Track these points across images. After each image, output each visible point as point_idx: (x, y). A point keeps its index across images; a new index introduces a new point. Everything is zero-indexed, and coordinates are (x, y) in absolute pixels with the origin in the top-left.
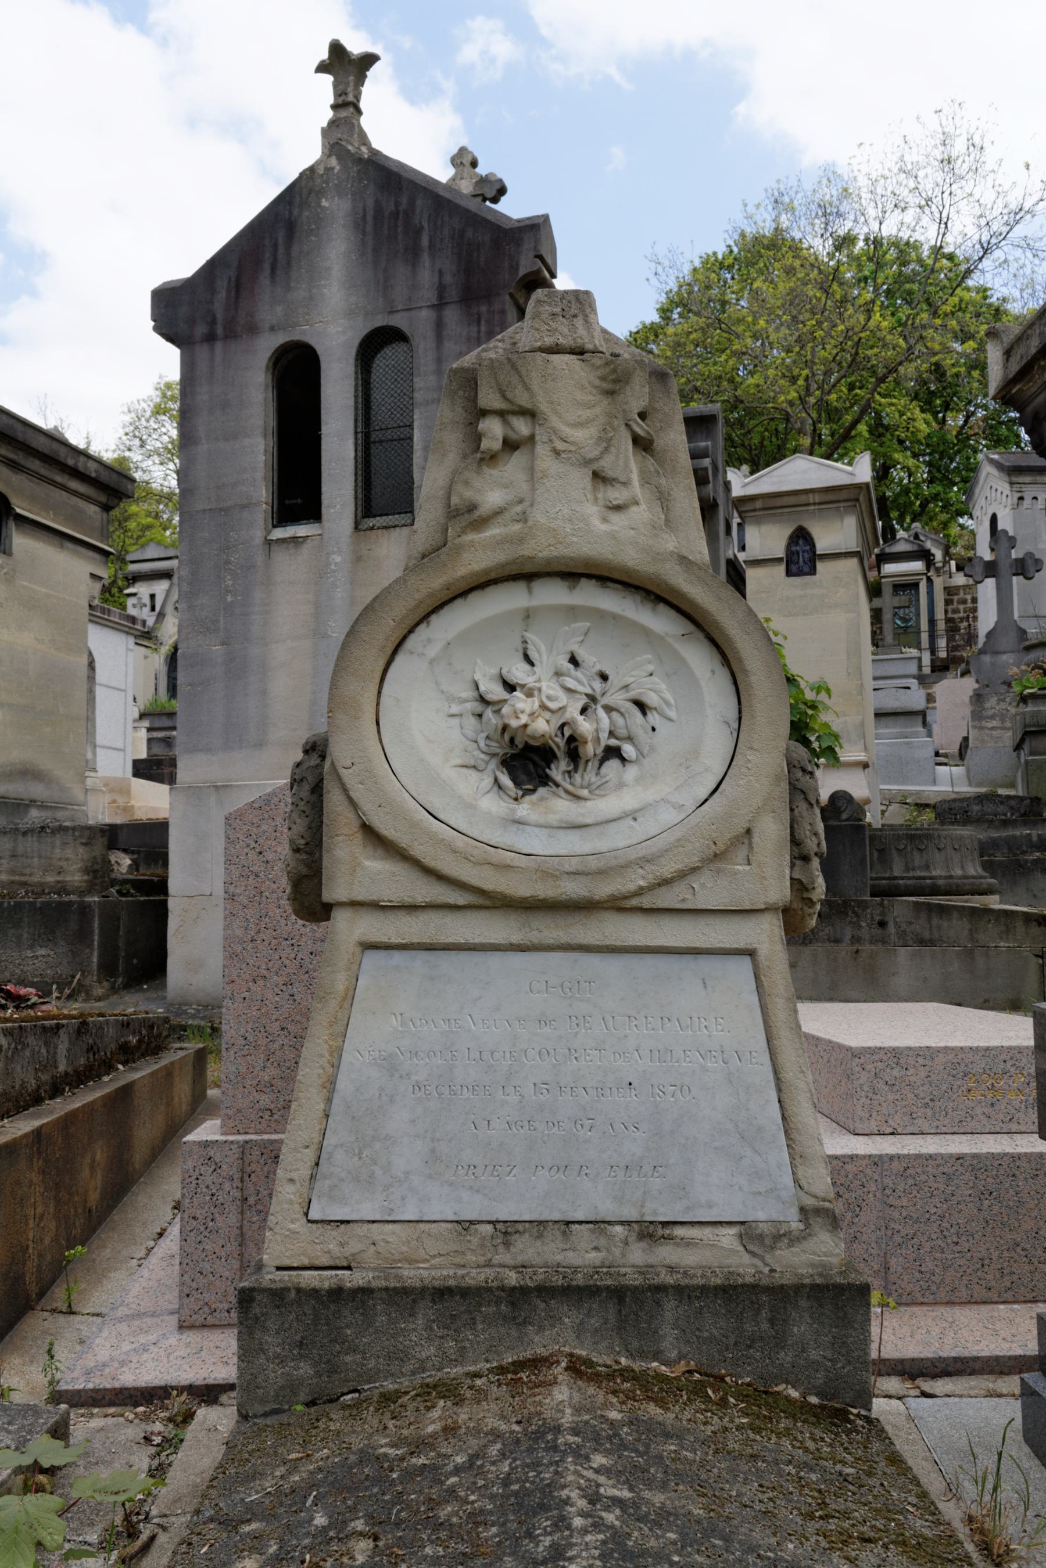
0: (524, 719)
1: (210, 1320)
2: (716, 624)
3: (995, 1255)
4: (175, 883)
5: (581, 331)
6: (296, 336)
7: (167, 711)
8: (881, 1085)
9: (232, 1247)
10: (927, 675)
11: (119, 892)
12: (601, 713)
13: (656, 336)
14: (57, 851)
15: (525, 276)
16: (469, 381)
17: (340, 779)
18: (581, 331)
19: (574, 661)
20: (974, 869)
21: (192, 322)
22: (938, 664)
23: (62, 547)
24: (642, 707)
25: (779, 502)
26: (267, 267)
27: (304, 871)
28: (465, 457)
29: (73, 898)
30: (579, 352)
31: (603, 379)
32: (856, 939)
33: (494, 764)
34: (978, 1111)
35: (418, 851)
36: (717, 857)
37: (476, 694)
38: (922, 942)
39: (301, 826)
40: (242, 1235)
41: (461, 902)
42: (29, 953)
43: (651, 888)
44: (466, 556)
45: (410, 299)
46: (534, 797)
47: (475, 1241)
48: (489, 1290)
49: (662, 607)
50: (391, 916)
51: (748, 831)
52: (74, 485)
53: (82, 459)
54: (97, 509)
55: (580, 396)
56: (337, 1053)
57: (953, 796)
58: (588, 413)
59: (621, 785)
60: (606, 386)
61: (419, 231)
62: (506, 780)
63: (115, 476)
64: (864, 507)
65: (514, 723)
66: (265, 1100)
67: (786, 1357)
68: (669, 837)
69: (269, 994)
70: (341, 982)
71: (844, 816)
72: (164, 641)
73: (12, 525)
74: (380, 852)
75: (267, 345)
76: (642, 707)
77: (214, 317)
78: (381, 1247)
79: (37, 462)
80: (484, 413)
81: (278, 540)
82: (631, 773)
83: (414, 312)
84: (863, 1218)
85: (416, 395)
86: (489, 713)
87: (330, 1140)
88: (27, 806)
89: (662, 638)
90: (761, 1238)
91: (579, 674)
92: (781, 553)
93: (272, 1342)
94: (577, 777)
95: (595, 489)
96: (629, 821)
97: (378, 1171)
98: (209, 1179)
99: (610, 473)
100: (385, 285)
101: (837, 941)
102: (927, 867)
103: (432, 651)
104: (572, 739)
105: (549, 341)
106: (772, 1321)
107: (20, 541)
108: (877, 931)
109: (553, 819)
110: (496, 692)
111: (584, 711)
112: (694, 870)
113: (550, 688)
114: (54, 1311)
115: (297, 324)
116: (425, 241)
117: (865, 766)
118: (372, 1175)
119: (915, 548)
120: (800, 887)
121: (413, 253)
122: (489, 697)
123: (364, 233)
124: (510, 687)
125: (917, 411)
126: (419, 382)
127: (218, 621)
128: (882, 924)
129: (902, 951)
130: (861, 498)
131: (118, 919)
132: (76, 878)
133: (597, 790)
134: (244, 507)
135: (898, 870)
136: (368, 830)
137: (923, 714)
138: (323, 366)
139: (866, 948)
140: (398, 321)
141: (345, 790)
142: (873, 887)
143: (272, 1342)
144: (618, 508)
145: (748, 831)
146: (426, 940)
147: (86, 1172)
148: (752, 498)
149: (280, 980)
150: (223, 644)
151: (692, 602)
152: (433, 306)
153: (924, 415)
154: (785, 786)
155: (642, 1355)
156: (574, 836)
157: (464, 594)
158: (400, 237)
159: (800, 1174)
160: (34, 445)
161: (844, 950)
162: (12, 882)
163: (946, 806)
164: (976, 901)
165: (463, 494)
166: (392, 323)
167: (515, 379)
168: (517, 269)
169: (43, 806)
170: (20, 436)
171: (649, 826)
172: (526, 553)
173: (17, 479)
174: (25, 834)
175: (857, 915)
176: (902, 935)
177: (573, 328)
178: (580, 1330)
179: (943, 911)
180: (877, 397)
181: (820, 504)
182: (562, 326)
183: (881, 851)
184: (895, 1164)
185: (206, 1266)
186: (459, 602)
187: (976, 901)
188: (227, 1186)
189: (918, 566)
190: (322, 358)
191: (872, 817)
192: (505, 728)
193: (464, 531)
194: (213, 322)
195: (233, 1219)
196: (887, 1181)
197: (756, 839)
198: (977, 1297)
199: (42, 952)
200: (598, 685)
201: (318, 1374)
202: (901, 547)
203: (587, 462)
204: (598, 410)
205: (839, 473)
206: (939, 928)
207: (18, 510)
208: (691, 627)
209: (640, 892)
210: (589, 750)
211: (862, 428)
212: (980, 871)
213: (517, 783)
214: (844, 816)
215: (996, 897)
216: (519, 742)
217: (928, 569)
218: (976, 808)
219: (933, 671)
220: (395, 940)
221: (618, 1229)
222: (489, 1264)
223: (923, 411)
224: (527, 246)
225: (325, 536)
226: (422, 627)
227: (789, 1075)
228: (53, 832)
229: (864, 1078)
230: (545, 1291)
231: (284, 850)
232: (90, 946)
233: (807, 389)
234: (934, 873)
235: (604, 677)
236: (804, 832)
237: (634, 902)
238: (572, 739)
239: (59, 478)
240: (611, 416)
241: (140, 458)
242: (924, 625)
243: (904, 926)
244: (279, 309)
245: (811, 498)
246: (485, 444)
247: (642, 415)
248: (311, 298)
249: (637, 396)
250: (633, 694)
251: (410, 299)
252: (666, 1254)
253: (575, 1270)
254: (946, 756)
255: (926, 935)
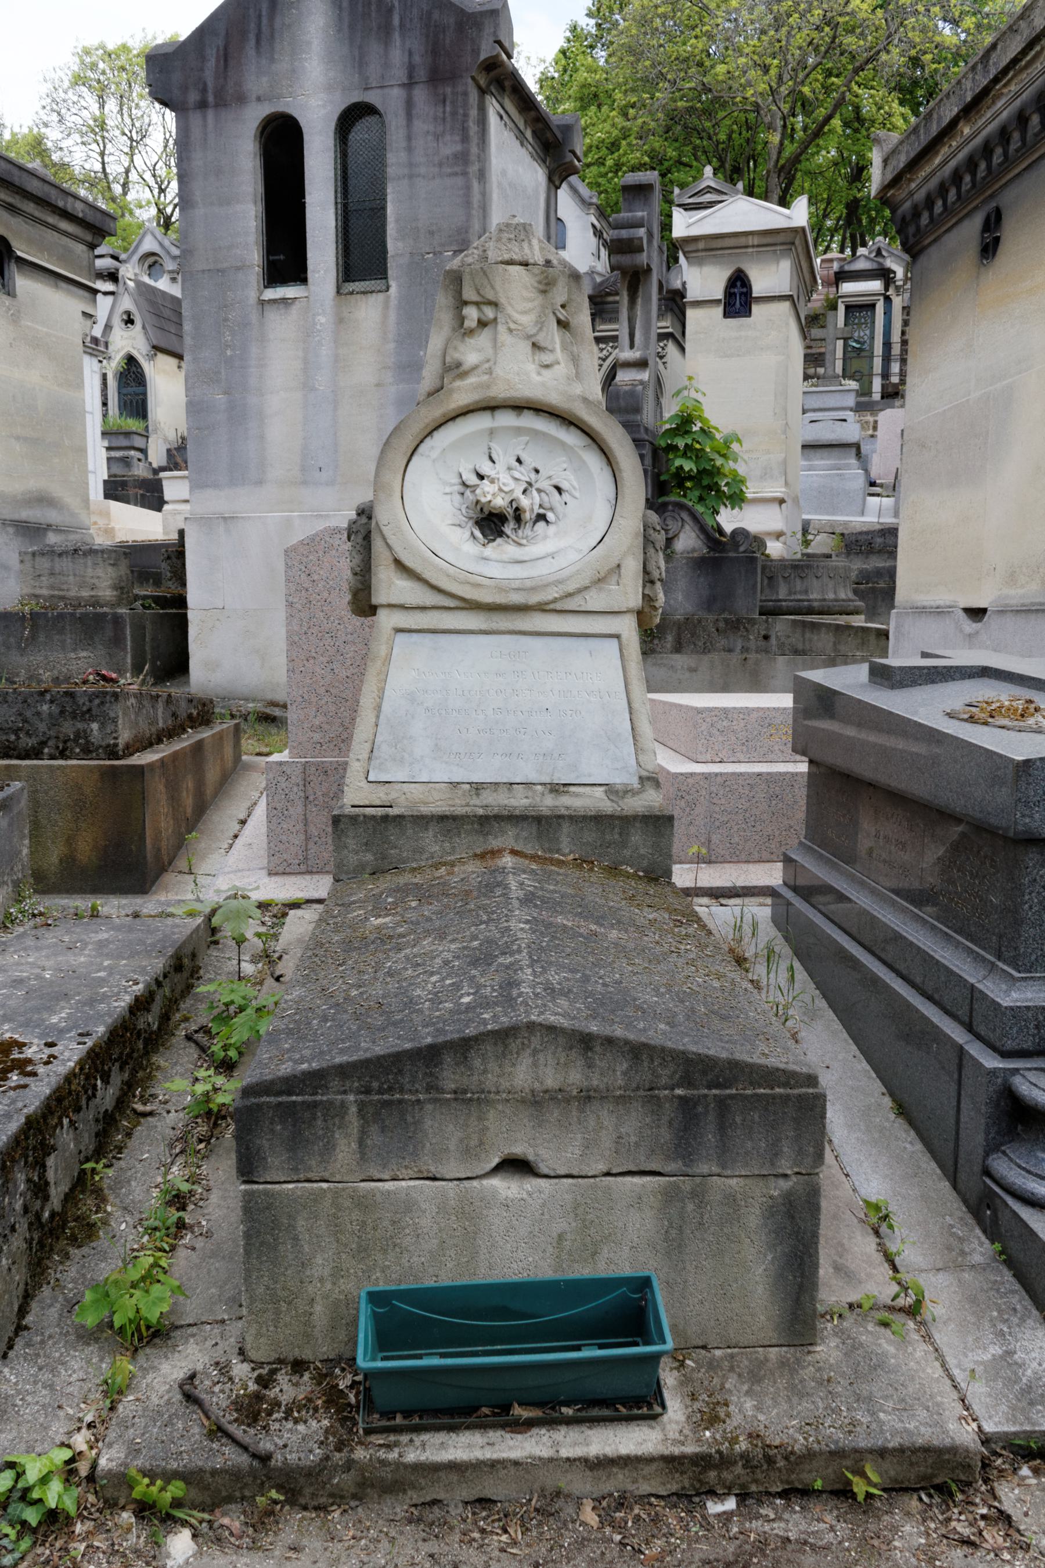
0: (489, 497)
1: (288, 870)
2: (604, 440)
3: (777, 833)
4: (194, 596)
5: (527, 251)
6: (280, 107)
7: (124, 429)
8: (715, 731)
9: (300, 826)
10: (877, 402)
11: (143, 605)
12: (535, 493)
13: (365, 1250)
14: (90, 570)
15: (486, 60)
16: (456, 279)
17: (381, 531)
18: (527, 251)
19: (519, 461)
20: (845, 593)
21: (185, 89)
22: (890, 390)
23: (57, 286)
24: (559, 489)
25: (720, 243)
26: (252, 42)
27: (360, 586)
28: (454, 330)
29: (105, 609)
30: (525, 264)
31: (540, 282)
32: (745, 649)
33: (471, 523)
34: (776, 748)
35: (427, 575)
36: (600, 581)
37: (459, 481)
38: (796, 652)
39: (357, 560)
40: (306, 819)
41: (452, 605)
42: (73, 655)
43: (562, 598)
44: (455, 396)
45: (383, 77)
46: (494, 544)
47: (460, 792)
48: (468, 817)
49: (572, 428)
50: (411, 613)
51: (619, 566)
52: (65, 225)
53: (70, 200)
54: (84, 248)
55: (525, 294)
56: (382, 690)
57: (878, 527)
58: (530, 305)
59: (546, 537)
60: (541, 287)
61: (390, 10)
62: (478, 533)
63: (99, 215)
64: (800, 249)
65: (483, 500)
66: (317, 737)
67: (627, 853)
68: (573, 569)
69: (318, 669)
70: (383, 651)
71: (742, 549)
72: (113, 355)
73: (13, 267)
74: (405, 575)
75: (254, 115)
76: (559, 489)
77: (205, 84)
78: (408, 795)
79: (32, 205)
80: (466, 303)
81: (270, 301)
82: (552, 529)
83: (386, 90)
84: (696, 811)
85: (389, 170)
86: (468, 493)
87: (379, 739)
88: (45, 529)
89: (571, 448)
90: (617, 792)
91: (522, 469)
92: (719, 295)
93: (351, 843)
94: (520, 532)
95: (533, 354)
96: (550, 559)
97: (406, 756)
98: (284, 785)
99: (542, 344)
100: (360, 62)
101: (730, 651)
102: (806, 592)
103: (435, 454)
104: (517, 509)
105: (506, 257)
106: (620, 834)
107: (23, 283)
108: (762, 643)
109: (505, 557)
110: (473, 480)
111: (524, 492)
112: (586, 588)
113: (505, 478)
114: (180, 872)
115: (279, 97)
116: (396, 21)
117: (782, 501)
118: (402, 758)
119: (875, 266)
120: (648, 599)
121: (385, 31)
122: (468, 483)
123: (340, 8)
124: (481, 477)
125: (895, 105)
126: (391, 158)
127: (219, 372)
128: (766, 638)
129: (781, 659)
130: (797, 242)
131: (144, 628)
132: (106, 593)
133: (531, 540)
134: (238, 269)
135: (782, 593)
136: (399, 564)
137: (857, 447)
138: (306, 138)
139: (752, 656)
140: (373, 98)
141: (384, 539)
142: (761, 607)
143: (351, 843)
144: (547, 366)
145: (619, 566)
146: (432, 627)
147: (184, 794)
148: (695, 239)
149: (325, 660)
150: (225, 393)
151: (589, 427)
152: (404, 85)
153: (902, 110)
154: (641, 539)
155: (550, 851)
156: (517, 567)
157: (453, 419)
158: (373, 14)
159: (640, 758)
160: (29, 189)
161: (735, 658)
162: (53, 596)
163: (854, 538)
164: (842, 620)
165: (453, 356)
166: (367, 100)
167: (486, 282)
168: (478, 54)
169: (58, 530)
170: (16, 181)
171: (560, 562)
172: (492, 395)
173: (16, 222)
174: (60, 555)
175: (747, 630)
176: (781, 646)
177: (522, 248)
178: (517, 838)
179: (814, 626)
180: (855, 88)
181: (758, 246)
182: (515, 247)
183: (770, 578)
184: (719, 779)
185: (284, 838)
186: (450, 423)
187: (842, 620)
188: (295, 789)
189: (876, 285)
190: (305, 130)
191: (774, 549)
192: (478, 502)
193: (454, 380)
194: (204, 90)
195: (300, 809)
196: (713, 789)
197: (623, 571)
198: (764, 858)
199: (84, 654)
200: (533, 475)
201: (376, 859)
202: (861, 265)
203: (529, 337)
204: (536, 303)
205: (777, 216)
206: (810, 640)
207: (19, 253)
208: (590, 441)
209: (555, 600)
210: (527, 516)
211: (836, 123)
212: (851, 595)
213: (485, 536)
214: (742, 549)
215: (862, 617)
216: (486, 511)
217: (887, 289)
218: (879, 540)
219: (883, 397)
220: (414, 627)
221: (539, 787)
222: (467, 805)
223: (902, 103)
224: (488, 30)
225: (311, 299)
226: (428, 439)
227: (636, 705)
228: (85, 554)
229: (704, 726)
230: (498, 818)
231: (347, 574)
232: (124, 649)
233: (780, 77)
234: (811, 597)
235: (537, 471)
236: (652, 567)
237: (551, 606)
238: (517, 509)
239: (51, 219)
240: (543, 307)
241: (60, 136)
242: (878, 349)
243: (783, 639)
244: (265, 79)
245: (751, 241)
246: (467, 324)
247: (563, 306)
248: (294, 71)
249: (560, 294)
250: (554, 482)
251: (383, 77)
252: (565, 801)
253: (515, 808)
254: (881, 486)
255: (800, 647)
